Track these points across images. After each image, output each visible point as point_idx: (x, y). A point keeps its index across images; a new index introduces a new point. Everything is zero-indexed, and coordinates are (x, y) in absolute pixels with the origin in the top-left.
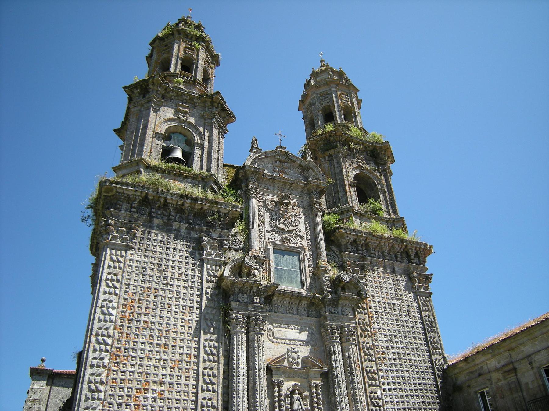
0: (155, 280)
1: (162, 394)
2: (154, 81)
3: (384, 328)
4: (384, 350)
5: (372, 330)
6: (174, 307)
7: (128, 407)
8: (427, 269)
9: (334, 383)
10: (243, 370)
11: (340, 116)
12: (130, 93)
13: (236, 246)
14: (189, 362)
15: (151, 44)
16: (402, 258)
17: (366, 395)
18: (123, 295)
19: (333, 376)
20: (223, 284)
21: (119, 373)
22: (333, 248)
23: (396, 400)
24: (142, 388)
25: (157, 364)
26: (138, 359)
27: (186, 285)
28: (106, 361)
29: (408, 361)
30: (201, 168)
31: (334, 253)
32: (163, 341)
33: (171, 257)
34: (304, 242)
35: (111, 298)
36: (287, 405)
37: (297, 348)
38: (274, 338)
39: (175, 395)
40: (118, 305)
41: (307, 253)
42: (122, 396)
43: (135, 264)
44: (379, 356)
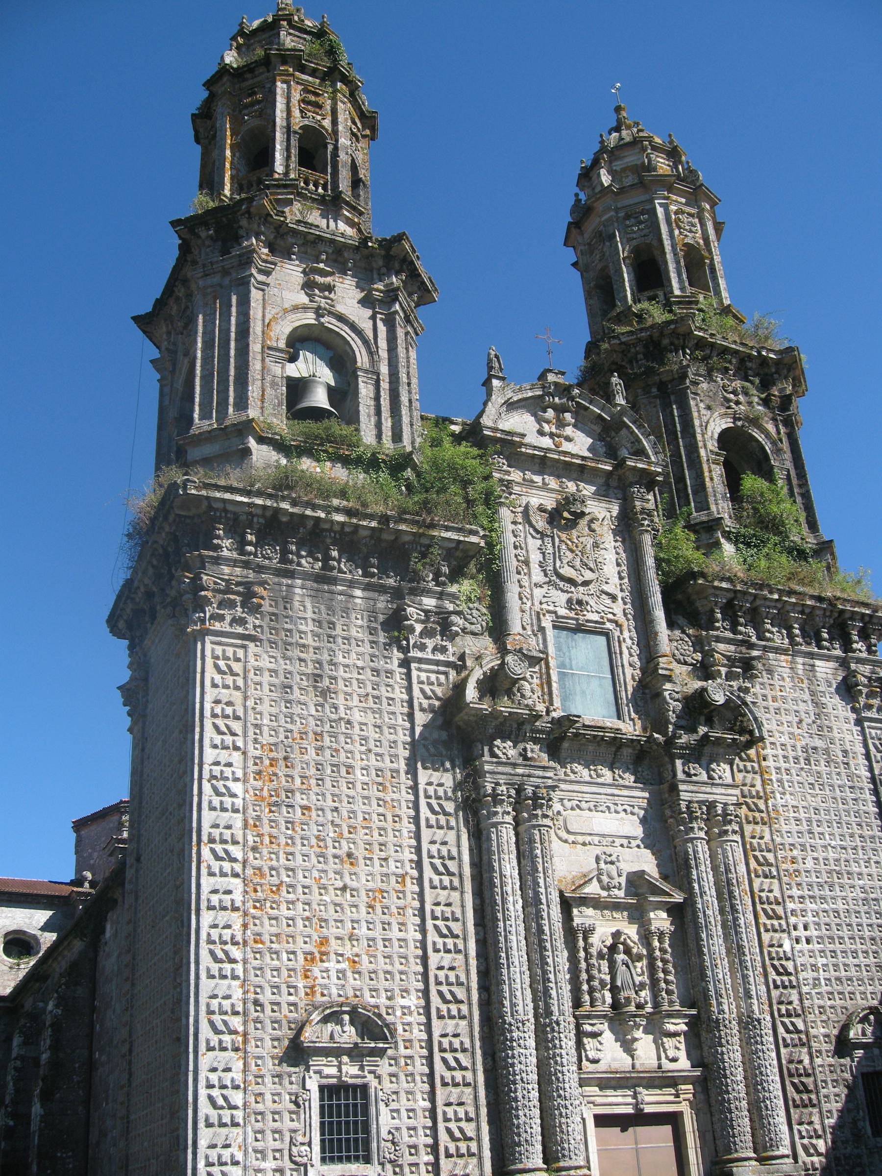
0: (313, 712)
1: (354, 962)
2: (252, 210)
3: (795, 803)
4: (795, 852)
5: (770, 808)
6: (358, 772)
7: (292, 990)
9: (697, 927)
10: (515, 905)
11: (679, 275)
12: (188, 236)
13: (472, 624)
14: (403, 892)
15: (208, 84)
17: (761, 952)
18: (252, 752)
20: (460, 718)
21: (266, 922)
23: (821, 961)
24: (315, 951)
25: (338, 900)
28: (238, 897)
29: (846, 876)
30: (379, 436)
34: (618, 608)
36: (603, 976)
37: (616, 851)
38: (568, 832)
39: (381, 964)
40: (245, 774)
41: (626, 634)
42: (278, 970)
43: (266, 678)
44: (784, 866)
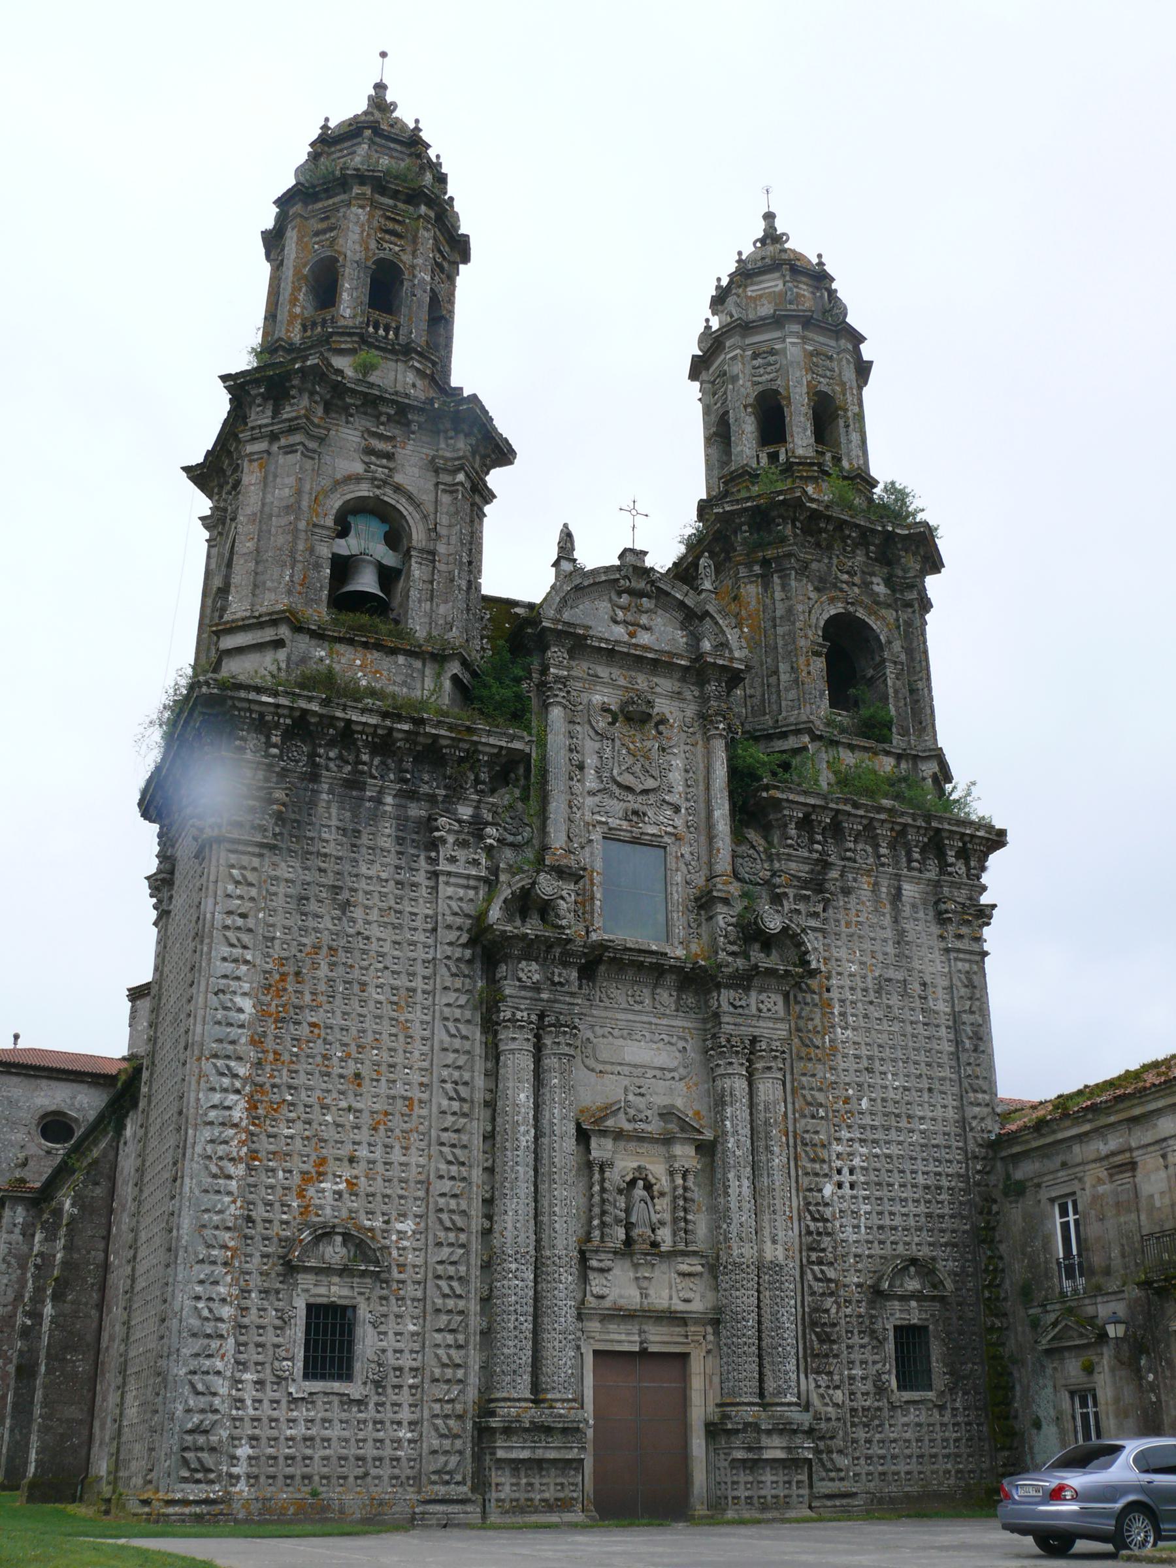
8: (984, 888)
16: (922, 862)
19: (724, 1151)
22: (752, 835)
26: (301, 1109)
27: (398, 938)
31: (753, 847)
32: (352, 1068)
33: (363, 869)
35: (238, 973)
42: (272, 1187)
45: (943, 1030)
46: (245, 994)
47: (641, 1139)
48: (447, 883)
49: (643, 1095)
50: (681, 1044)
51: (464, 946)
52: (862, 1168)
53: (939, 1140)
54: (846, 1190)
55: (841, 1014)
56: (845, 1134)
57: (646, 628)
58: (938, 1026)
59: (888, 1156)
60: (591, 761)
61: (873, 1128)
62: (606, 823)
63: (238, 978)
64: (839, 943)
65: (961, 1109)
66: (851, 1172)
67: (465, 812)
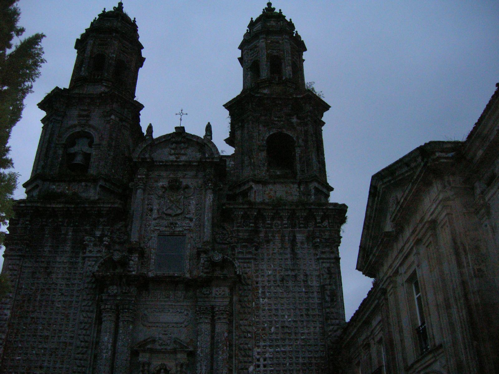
45: (315, 294)
46: (8, 309)
47: (164, 353)
48: (89, 261)
49: (166, 334)
50: (186, 312)
51: (94, 283)
52: (270, 358)
53: (312, 342)
54: (262, 368)
55: (262, 292)
56: (262, 344)
57: (183, 155)
58: (313, 292)
59: (285, 352)
60: (155, 207)
61: (277, 340)
62: (159, 229)
63: (6, 304)
64: (263, 263)
65: (322, 328)
66: (265, 360)
67: (98, 233)
